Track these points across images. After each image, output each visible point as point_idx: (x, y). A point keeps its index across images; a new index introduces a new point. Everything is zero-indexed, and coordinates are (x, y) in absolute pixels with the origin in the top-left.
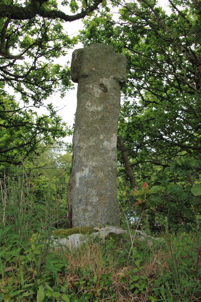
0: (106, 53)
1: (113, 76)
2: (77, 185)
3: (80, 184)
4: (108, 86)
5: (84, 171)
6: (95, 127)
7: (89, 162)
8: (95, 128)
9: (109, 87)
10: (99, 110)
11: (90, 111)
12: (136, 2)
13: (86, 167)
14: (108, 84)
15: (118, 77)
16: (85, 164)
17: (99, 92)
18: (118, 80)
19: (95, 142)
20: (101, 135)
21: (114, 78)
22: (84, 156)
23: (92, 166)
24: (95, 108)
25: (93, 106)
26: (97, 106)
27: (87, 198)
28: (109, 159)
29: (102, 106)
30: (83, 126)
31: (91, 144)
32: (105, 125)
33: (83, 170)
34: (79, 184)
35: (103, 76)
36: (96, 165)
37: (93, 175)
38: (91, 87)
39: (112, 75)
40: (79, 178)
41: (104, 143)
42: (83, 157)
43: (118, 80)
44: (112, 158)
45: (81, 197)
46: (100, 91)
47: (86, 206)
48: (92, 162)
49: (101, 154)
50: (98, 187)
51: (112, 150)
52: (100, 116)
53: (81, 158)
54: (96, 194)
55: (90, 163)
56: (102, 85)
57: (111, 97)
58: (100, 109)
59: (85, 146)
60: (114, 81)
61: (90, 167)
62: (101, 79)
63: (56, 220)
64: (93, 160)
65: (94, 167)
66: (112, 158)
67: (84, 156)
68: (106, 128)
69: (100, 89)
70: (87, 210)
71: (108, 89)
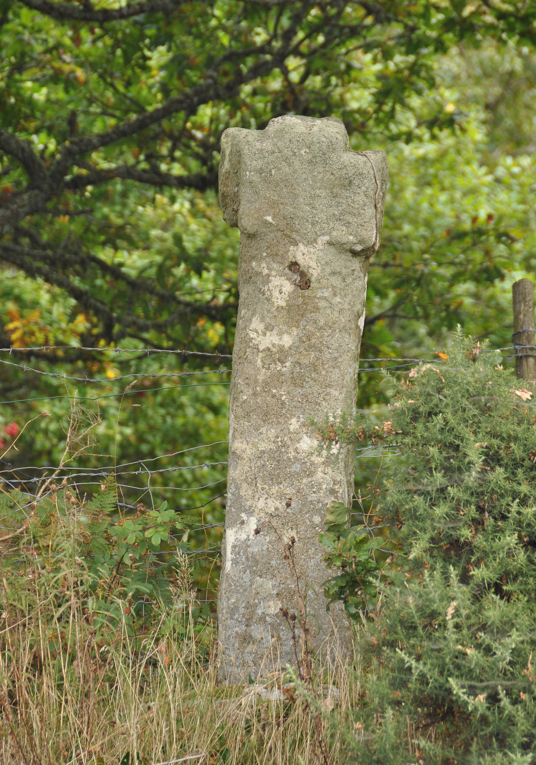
0: (310, 162)
1: (326, 238)
2: (228, 566)
3: (235, 562)
4: (311, 271)
5: (245, 526)
6: (274, 396)
7: (259, 499)
8: (274, 400)
9: (314, 273)
10: (287, 345)
11: (261, 348)
12: (8, 760)
13: (250, 512)
14: (313, 264)
15: (345, 240)
16: (249, 503)
17: (284, 289)
18: (345, 246)
19: (274, 442)
20: (294, 421)
21: (330, 243)
22: (246, 480)
23: (267, 510)
24: (275, 340)
25: (268, 334)
26: (280, 334)
27: (251, 607)
28: (314, 490)
29: (295, 331)
30: (242, 392)
31: (263, 446)
32: (304, 390)
33: (243, 523)
34: (231, 562)
35: (298, 238)
36: (277, 509)
37: (268, 538)
38: (266, 271)
39: (323, 234)
40: (231, 544)
41: (301, 441)
42: (245, 485)
43: (345, 246)
44: (324, 487)
45: (238, 600)
46: (288, 287)
47: (247, 626)
48: (267, 499)
49: (291, 476)
50: (281, 571)
51: (323, 463)
52: (288, 364)
53: (238, 488)
54: (275, 592)
55: (261, 504)
56: (294, 266)
57: (322, 304)
58: (287, 341)
59: (248, 452)
60: (332, 250)
61: (262, 515)
62: (292, 248)
63: (525, 315)
64: (267, 494)
65: (271, 514)
66: (324, 487)
67: (246, 480)
68: (306, 396)
69: (289, 279)
70: (251, 636)
71: (313, 279)
